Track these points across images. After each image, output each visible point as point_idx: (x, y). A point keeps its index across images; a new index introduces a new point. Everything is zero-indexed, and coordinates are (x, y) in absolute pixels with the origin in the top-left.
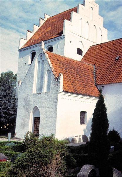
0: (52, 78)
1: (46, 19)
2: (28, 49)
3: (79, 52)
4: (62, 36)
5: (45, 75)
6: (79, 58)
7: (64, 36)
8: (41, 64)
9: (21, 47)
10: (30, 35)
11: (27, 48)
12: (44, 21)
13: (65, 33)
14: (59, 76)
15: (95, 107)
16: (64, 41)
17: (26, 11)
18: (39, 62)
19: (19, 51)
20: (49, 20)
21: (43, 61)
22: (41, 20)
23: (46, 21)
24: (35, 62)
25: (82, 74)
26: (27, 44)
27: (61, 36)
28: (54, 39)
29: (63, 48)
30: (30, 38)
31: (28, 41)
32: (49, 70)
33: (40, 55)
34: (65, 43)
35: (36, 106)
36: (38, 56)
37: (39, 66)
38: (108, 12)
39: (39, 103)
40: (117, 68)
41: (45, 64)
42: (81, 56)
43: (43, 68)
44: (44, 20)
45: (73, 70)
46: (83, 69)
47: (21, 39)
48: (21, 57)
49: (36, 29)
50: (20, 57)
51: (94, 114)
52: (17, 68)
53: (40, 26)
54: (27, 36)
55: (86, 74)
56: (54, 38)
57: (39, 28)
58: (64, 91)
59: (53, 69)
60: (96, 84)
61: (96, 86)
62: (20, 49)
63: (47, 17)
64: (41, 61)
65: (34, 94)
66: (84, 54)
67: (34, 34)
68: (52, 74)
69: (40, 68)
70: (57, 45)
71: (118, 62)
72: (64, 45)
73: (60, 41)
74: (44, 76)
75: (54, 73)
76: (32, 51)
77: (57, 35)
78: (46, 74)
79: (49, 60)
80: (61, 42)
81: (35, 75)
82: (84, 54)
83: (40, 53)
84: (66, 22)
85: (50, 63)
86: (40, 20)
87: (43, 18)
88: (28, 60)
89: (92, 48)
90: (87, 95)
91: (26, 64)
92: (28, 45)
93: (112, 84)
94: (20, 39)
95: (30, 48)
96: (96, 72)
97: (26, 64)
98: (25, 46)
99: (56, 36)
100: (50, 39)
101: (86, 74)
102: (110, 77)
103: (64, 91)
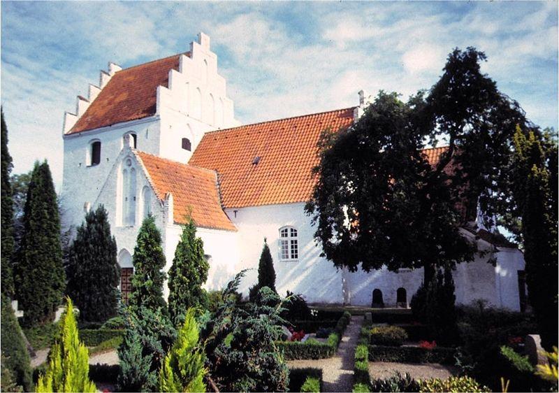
0: (153, 200)
1: (112, 74)
2: (85, 135)
3: (186, 144)
4: (154, 117)
5: (139, 195)
6: (184, 157)
7: (158, 116)
8: (129, 175)
9: (68, 130)
10: (84, 107)
11: (82, 133)
12: (109, 78)
13: (161, 109)
14: (166, 197)
15: (260, 258)
16: (159, 125)
17: (22, 11)
18: (125, 171)
19: (64, 138)
20: (118, 77)
21: (133, 169)
22: (104, 76)
23: (113, 78)
24: (117, 172)
25: (198, 190)
26: (79, 124)
27: (152, 115)
28: (138, 120)
29: (158, 139)
30: (84, 113)
31: (80, 117)
32: (146, 187)
33: (127, 159)
34: (161, 130)
35: (124, 249)
36: (123, 160)
37: (125, 177)
38: (215, 25)
39: (130, 243)
40: (257, 179)
41: (139, 175)
42: (188, 152)
43: (134, 182)
44: (109, 75)
45: (183, 183)
46: (200, 180)
47: (67, 114)
48: (69, 150)
49: (95, 93)
50: (66, 149)
51: (260, 265)
52: (62, 172)
53: (102, 87)
54: (77, 109)
55: (205, 189)
56: (139, 119)
57: (101, 91)
58: (175, 223)
59: (153, 184)
60: (222, 206)
61: (223, 209)
62: (67, 135)
63: (115, 69)
64: (129, 169)
65: (118, 228)
66: (194, 147)
67: (90, 104)
68: (152, 194)
69: (129, 183)
70: (145, 133)
71: (259, 168)
72: (159, 133)
73: (153, 125)
74: (137, 197)
75: (157, 191)
76: (93, 140)
77: (144, 112)
78: (141, 194)
79: (144, 168)
80: (152, 126)
81: (118, 193)
82: (194, 147)
83: (127, 154)
84: (162, 90)
85: (147, 173)
86: (101, 74)
87: (107, 71)
88: (84, 158)
89: (209, 138)
90: (210, 228)
91: (80, 164)
92: (82, 128)
93: (251, 208)
94: (65, 114)
95: (89, 134)
96: (219, 185)
97: (80, 164)
98: (78, 130)
99: (143, 115)
100: (131, 120)
101: (205, 189)
102: (246, 194)
103: (175, 223)
